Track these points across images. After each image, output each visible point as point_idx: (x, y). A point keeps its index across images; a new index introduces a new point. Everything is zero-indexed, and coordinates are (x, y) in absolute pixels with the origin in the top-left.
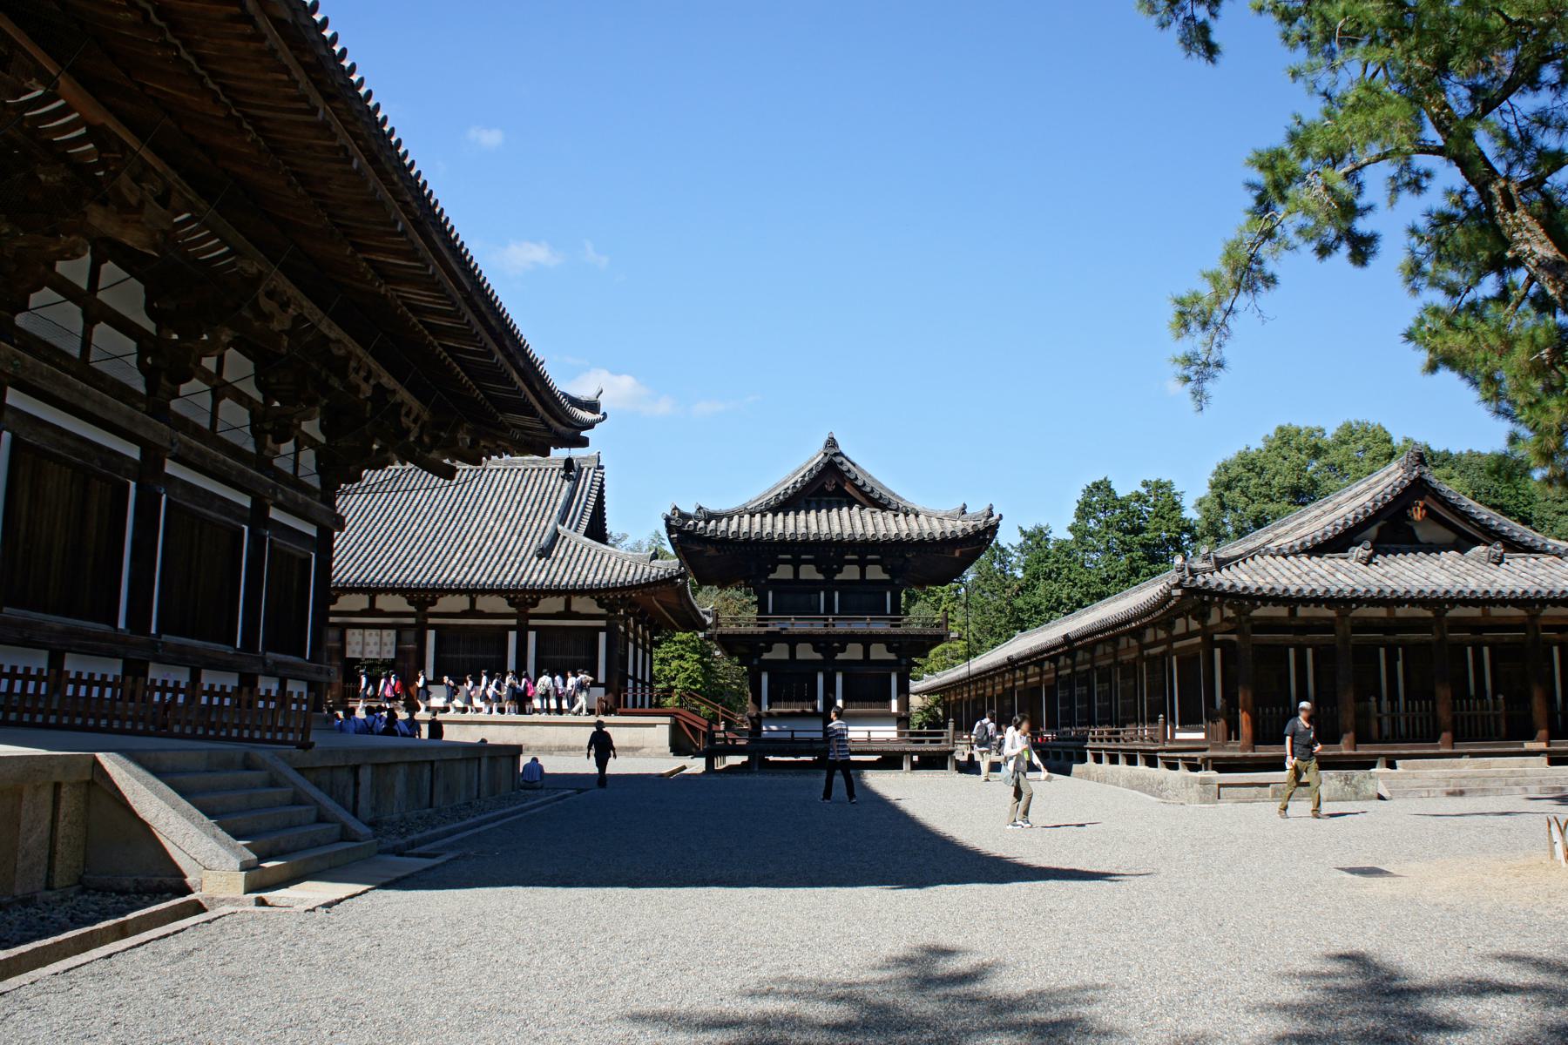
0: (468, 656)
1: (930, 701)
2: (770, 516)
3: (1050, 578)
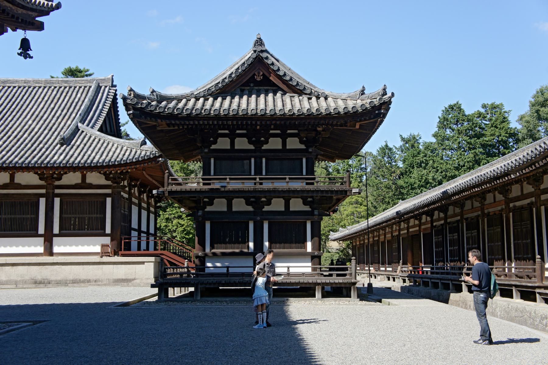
0: (9, 216)
1: (344, 245)
2: (211, 99)
3: (421, 166)
